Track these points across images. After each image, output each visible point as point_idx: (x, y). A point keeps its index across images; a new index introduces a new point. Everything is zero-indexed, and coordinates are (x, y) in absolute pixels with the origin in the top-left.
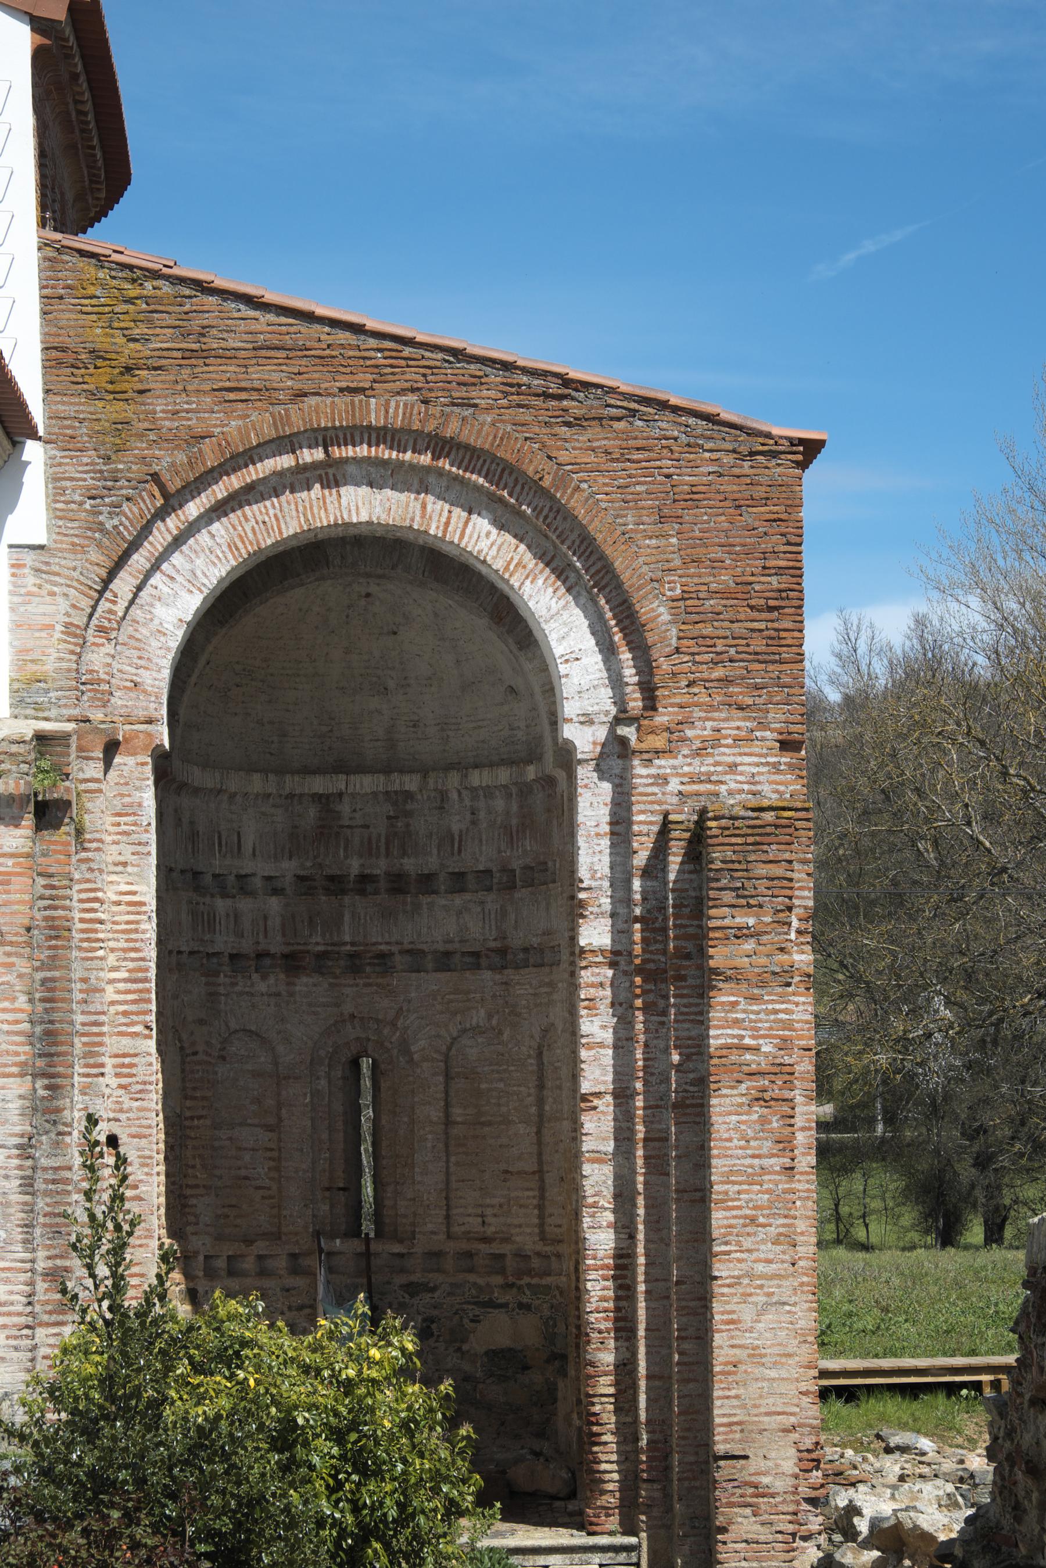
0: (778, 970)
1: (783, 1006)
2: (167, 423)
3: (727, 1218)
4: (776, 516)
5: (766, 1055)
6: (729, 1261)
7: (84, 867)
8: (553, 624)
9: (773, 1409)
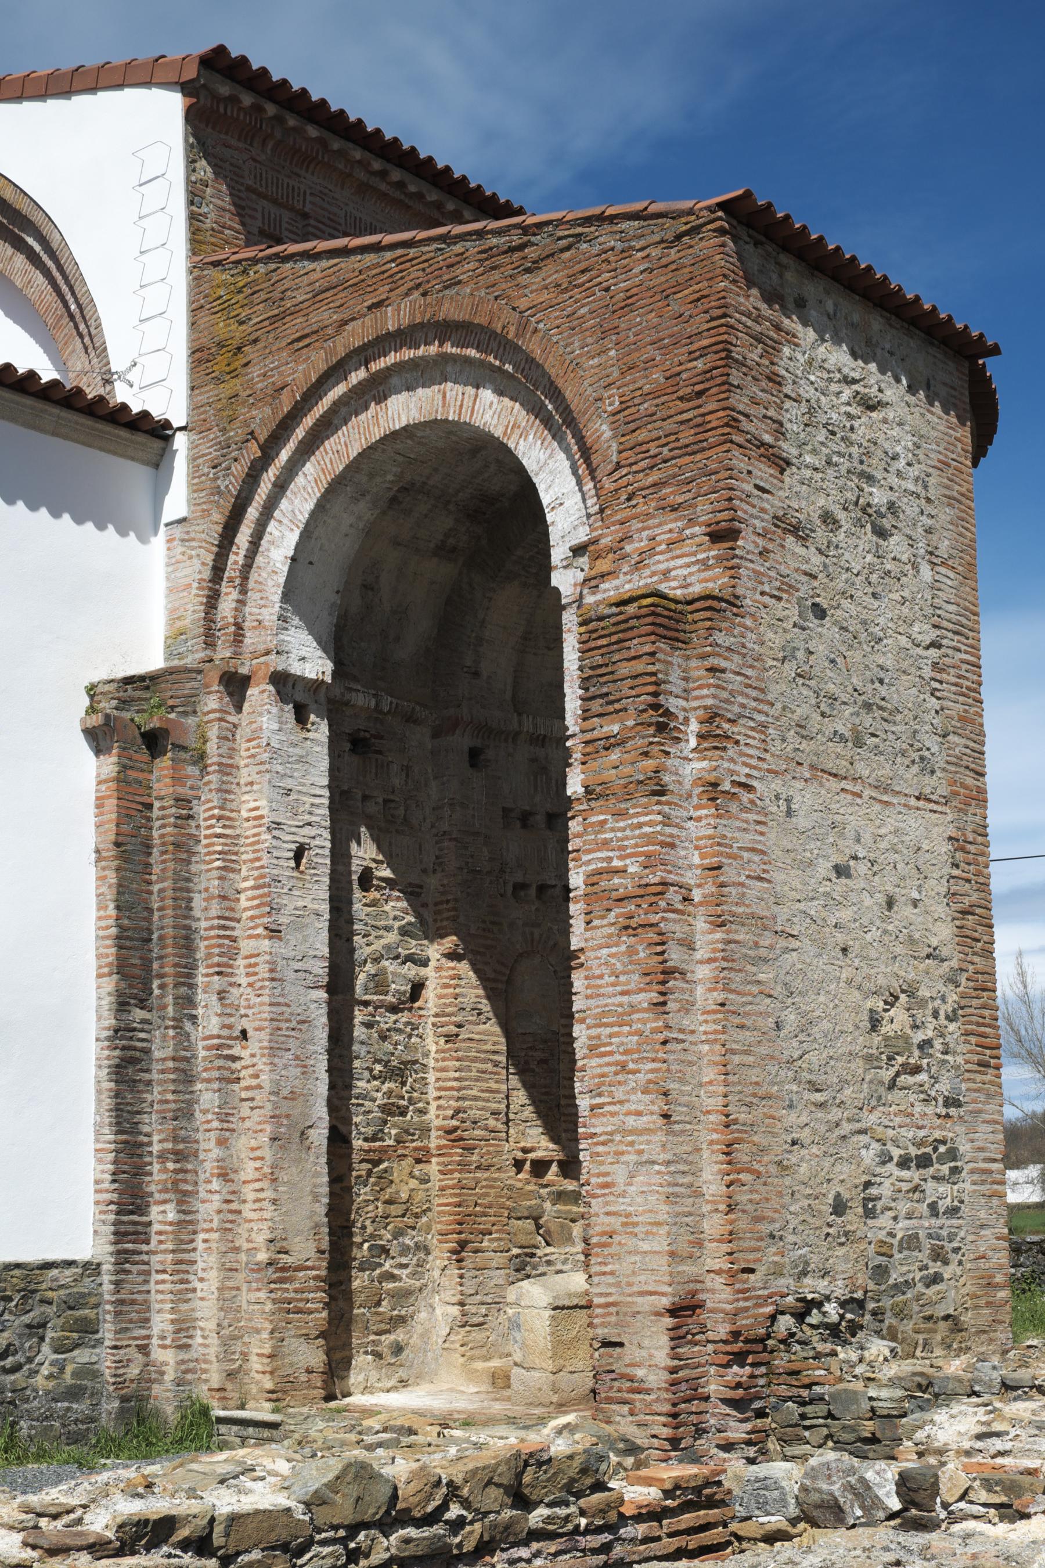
0: (641, 777)
1: (647, 819)
3: (600, 1066)
4: (698, 295)
5: (633, 876)
9: (646, 1288)
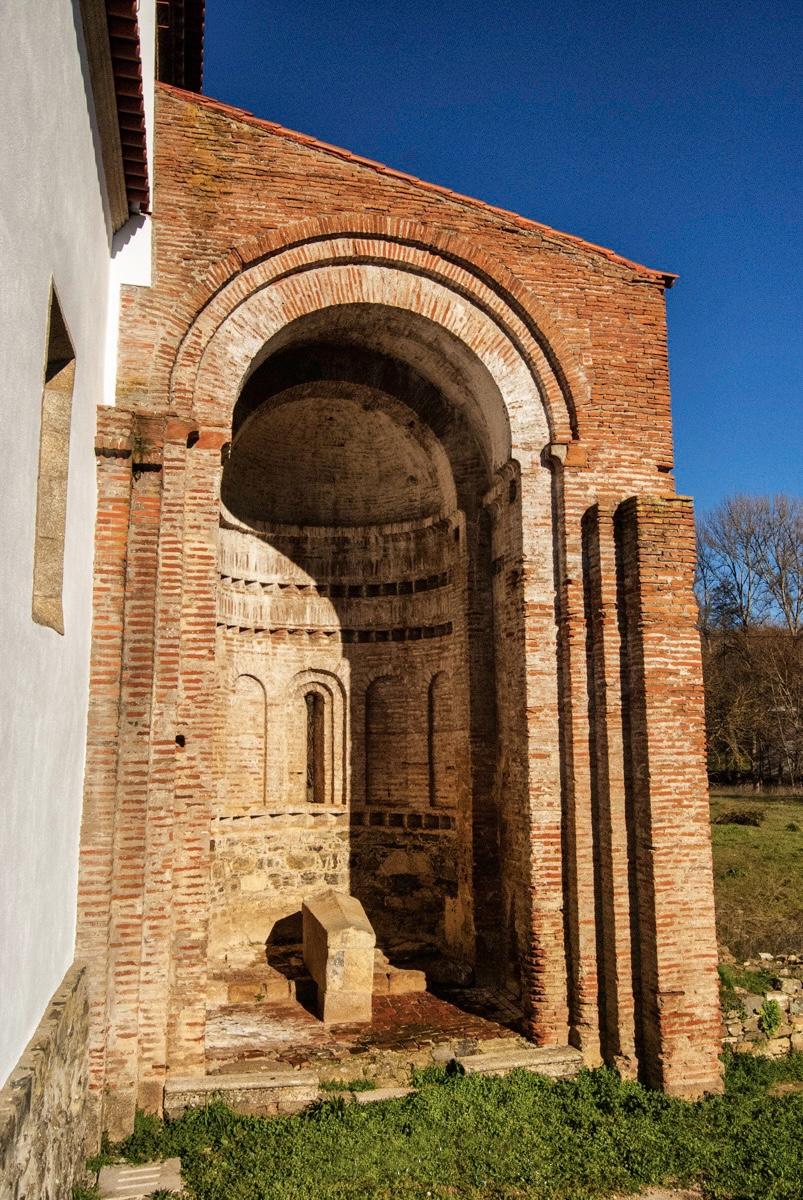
2: (244, 216)
6: (664, 835)
7: (168, 524)
8: (503, 382)
9: (700, 952)
